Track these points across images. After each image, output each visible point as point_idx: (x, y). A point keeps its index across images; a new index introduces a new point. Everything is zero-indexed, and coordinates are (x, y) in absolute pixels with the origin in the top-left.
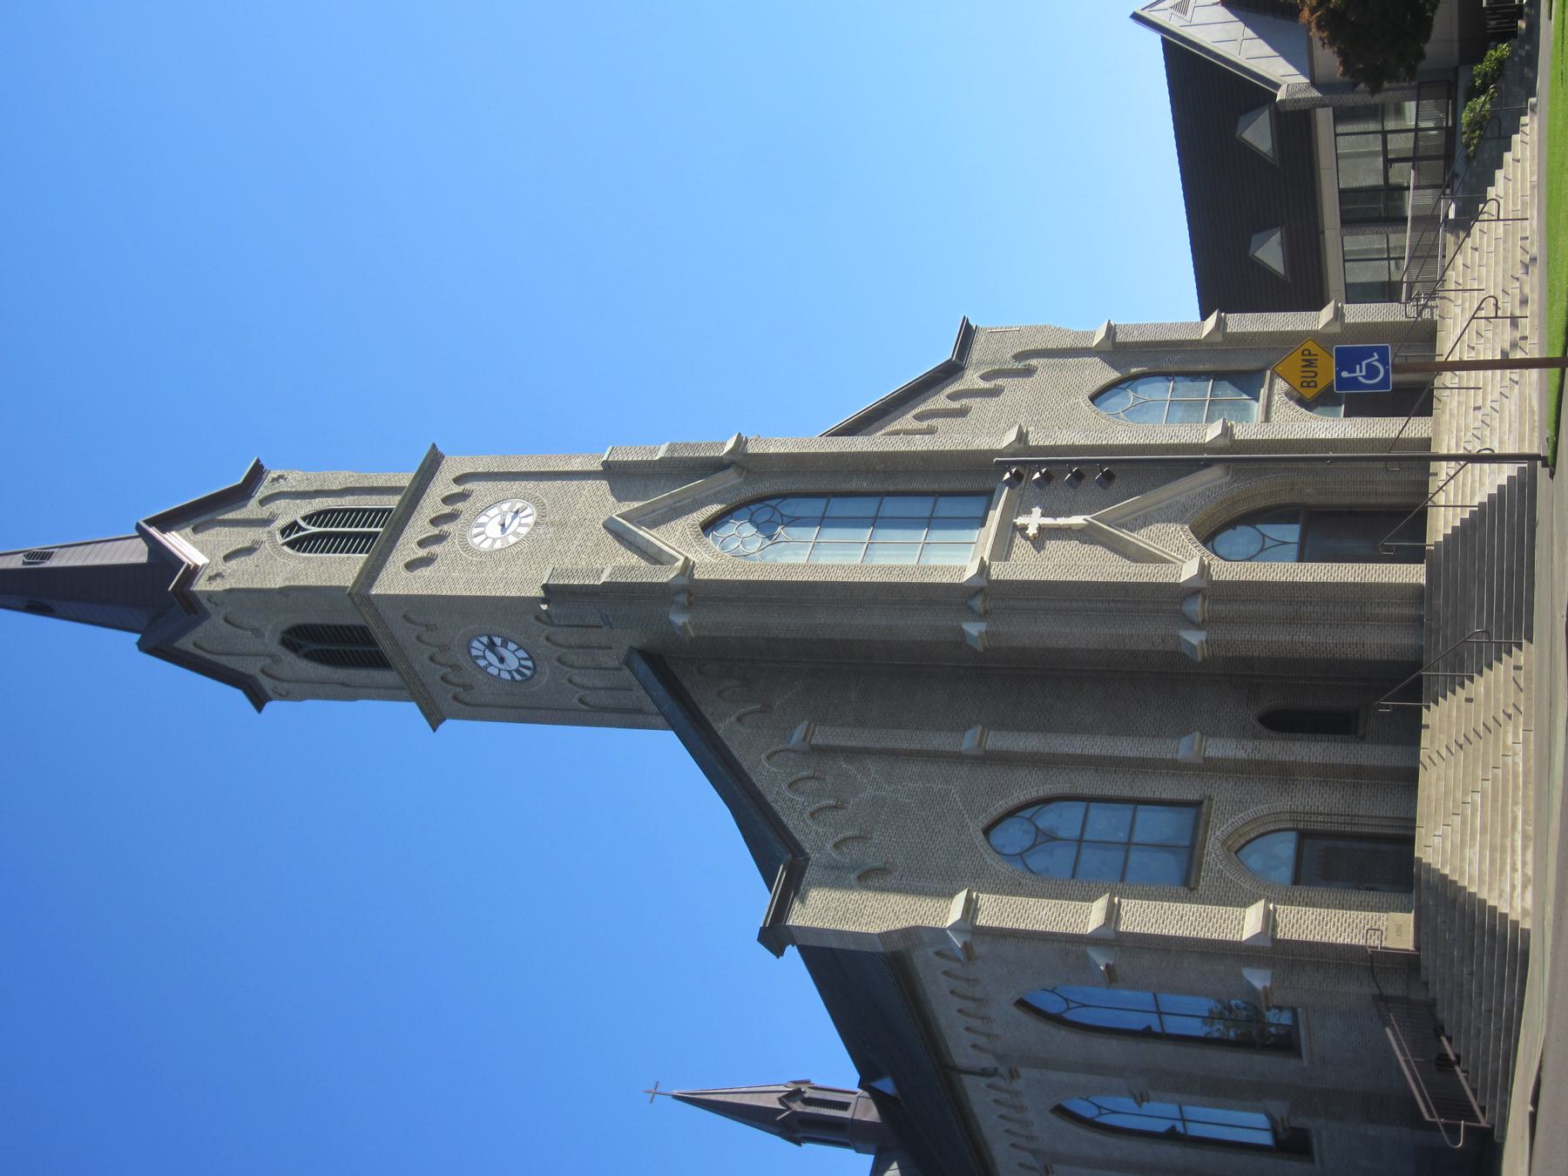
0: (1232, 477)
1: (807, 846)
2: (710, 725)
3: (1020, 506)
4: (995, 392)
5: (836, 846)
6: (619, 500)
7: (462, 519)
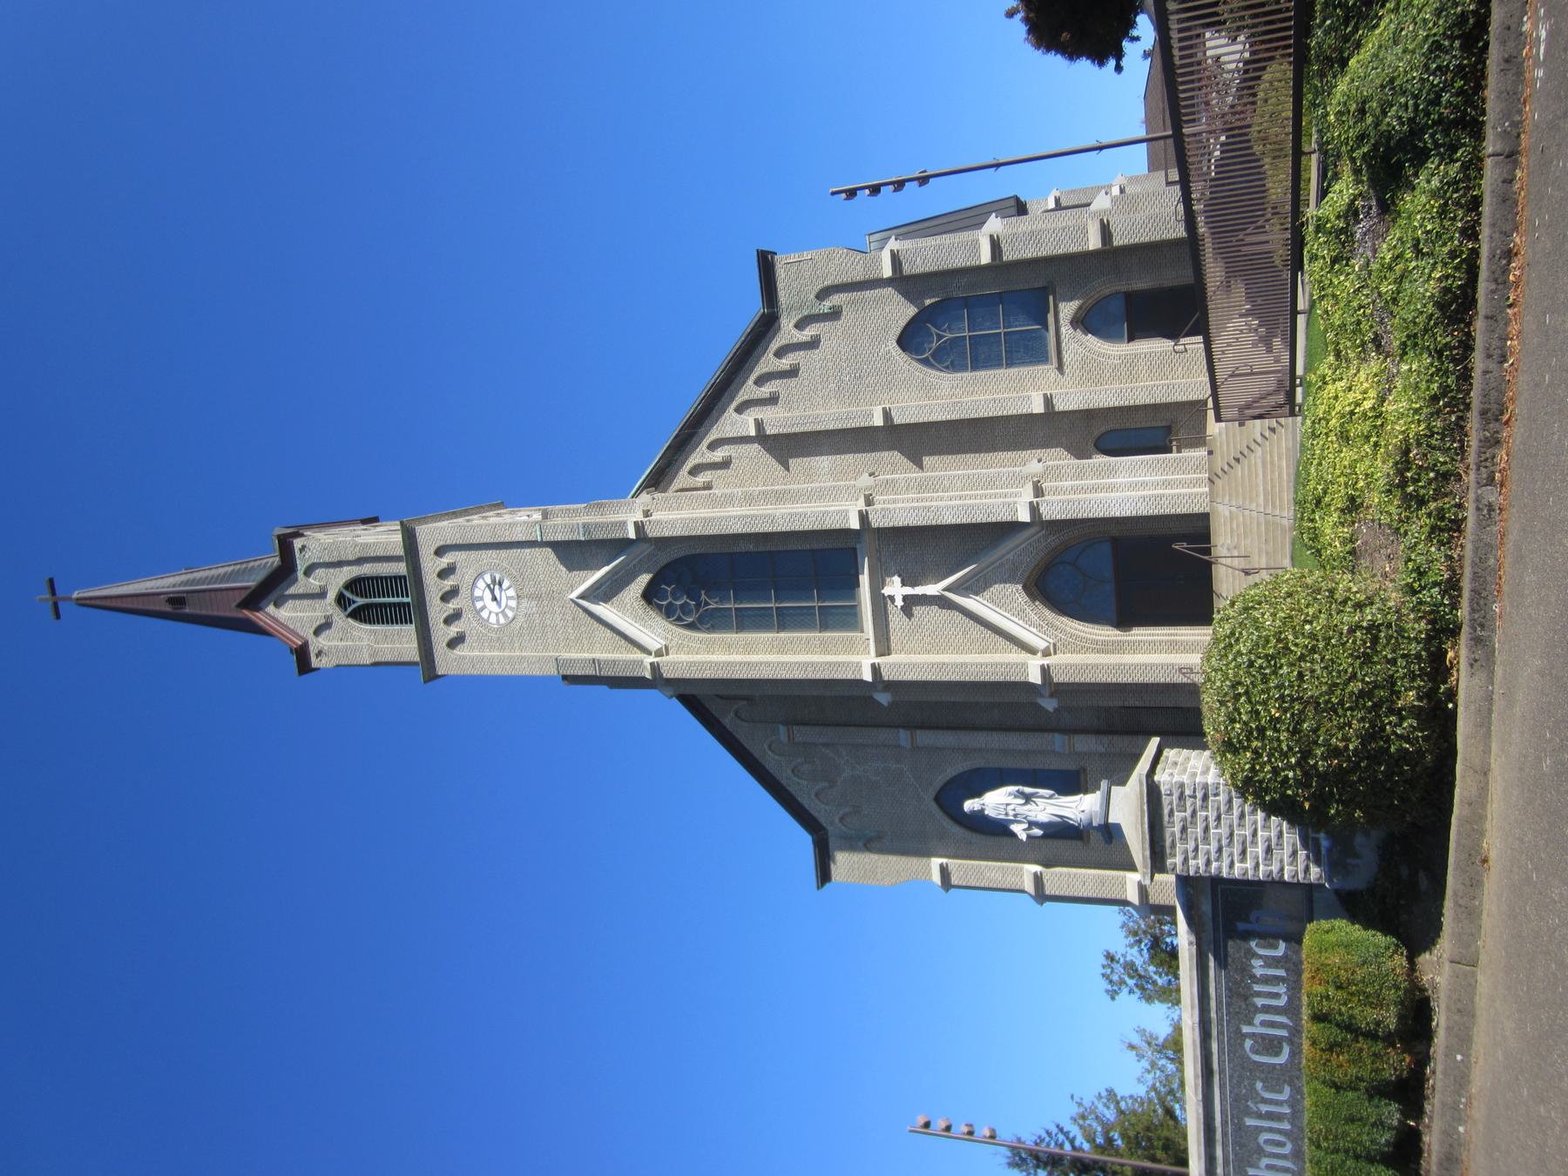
0: (1047, 529)
1: (823, 821)
2: (719, 722)
3: (879, 540)
4: (813, 344)
5: (841, 819)
6: (570, 568)
7: (464, 592)
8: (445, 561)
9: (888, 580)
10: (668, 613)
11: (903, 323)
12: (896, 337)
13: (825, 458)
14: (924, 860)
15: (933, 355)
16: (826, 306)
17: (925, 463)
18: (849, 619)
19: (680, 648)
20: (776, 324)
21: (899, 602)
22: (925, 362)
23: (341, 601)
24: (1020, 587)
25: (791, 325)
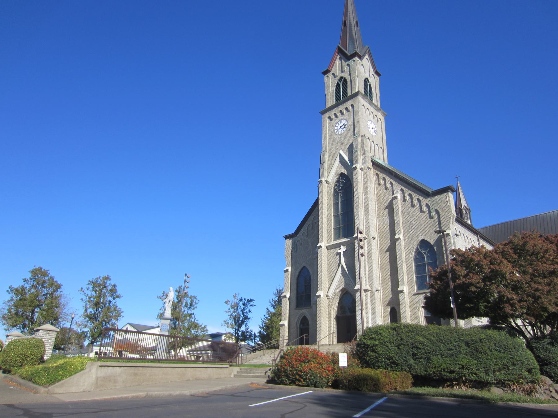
7: (343, 117)
8: (350, 108)
9: (345, 247)
10: (338, 181)
11: (428, 240)
12: (424, 238)
13: (388, 221)
14: (290, 265)
15: (419, 251)
16: (434, 213)
17: (387, 253)
18: (337, 237)
19: (328, 187)
20: (427, 197)
21: (339, 251)
22: (417, 249)
23: (341, 78)
24: (344, 287)
25: (427, 202)
